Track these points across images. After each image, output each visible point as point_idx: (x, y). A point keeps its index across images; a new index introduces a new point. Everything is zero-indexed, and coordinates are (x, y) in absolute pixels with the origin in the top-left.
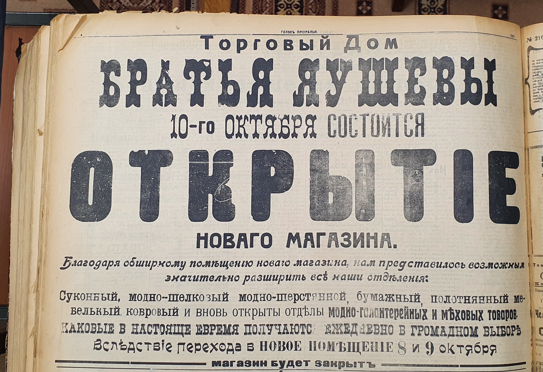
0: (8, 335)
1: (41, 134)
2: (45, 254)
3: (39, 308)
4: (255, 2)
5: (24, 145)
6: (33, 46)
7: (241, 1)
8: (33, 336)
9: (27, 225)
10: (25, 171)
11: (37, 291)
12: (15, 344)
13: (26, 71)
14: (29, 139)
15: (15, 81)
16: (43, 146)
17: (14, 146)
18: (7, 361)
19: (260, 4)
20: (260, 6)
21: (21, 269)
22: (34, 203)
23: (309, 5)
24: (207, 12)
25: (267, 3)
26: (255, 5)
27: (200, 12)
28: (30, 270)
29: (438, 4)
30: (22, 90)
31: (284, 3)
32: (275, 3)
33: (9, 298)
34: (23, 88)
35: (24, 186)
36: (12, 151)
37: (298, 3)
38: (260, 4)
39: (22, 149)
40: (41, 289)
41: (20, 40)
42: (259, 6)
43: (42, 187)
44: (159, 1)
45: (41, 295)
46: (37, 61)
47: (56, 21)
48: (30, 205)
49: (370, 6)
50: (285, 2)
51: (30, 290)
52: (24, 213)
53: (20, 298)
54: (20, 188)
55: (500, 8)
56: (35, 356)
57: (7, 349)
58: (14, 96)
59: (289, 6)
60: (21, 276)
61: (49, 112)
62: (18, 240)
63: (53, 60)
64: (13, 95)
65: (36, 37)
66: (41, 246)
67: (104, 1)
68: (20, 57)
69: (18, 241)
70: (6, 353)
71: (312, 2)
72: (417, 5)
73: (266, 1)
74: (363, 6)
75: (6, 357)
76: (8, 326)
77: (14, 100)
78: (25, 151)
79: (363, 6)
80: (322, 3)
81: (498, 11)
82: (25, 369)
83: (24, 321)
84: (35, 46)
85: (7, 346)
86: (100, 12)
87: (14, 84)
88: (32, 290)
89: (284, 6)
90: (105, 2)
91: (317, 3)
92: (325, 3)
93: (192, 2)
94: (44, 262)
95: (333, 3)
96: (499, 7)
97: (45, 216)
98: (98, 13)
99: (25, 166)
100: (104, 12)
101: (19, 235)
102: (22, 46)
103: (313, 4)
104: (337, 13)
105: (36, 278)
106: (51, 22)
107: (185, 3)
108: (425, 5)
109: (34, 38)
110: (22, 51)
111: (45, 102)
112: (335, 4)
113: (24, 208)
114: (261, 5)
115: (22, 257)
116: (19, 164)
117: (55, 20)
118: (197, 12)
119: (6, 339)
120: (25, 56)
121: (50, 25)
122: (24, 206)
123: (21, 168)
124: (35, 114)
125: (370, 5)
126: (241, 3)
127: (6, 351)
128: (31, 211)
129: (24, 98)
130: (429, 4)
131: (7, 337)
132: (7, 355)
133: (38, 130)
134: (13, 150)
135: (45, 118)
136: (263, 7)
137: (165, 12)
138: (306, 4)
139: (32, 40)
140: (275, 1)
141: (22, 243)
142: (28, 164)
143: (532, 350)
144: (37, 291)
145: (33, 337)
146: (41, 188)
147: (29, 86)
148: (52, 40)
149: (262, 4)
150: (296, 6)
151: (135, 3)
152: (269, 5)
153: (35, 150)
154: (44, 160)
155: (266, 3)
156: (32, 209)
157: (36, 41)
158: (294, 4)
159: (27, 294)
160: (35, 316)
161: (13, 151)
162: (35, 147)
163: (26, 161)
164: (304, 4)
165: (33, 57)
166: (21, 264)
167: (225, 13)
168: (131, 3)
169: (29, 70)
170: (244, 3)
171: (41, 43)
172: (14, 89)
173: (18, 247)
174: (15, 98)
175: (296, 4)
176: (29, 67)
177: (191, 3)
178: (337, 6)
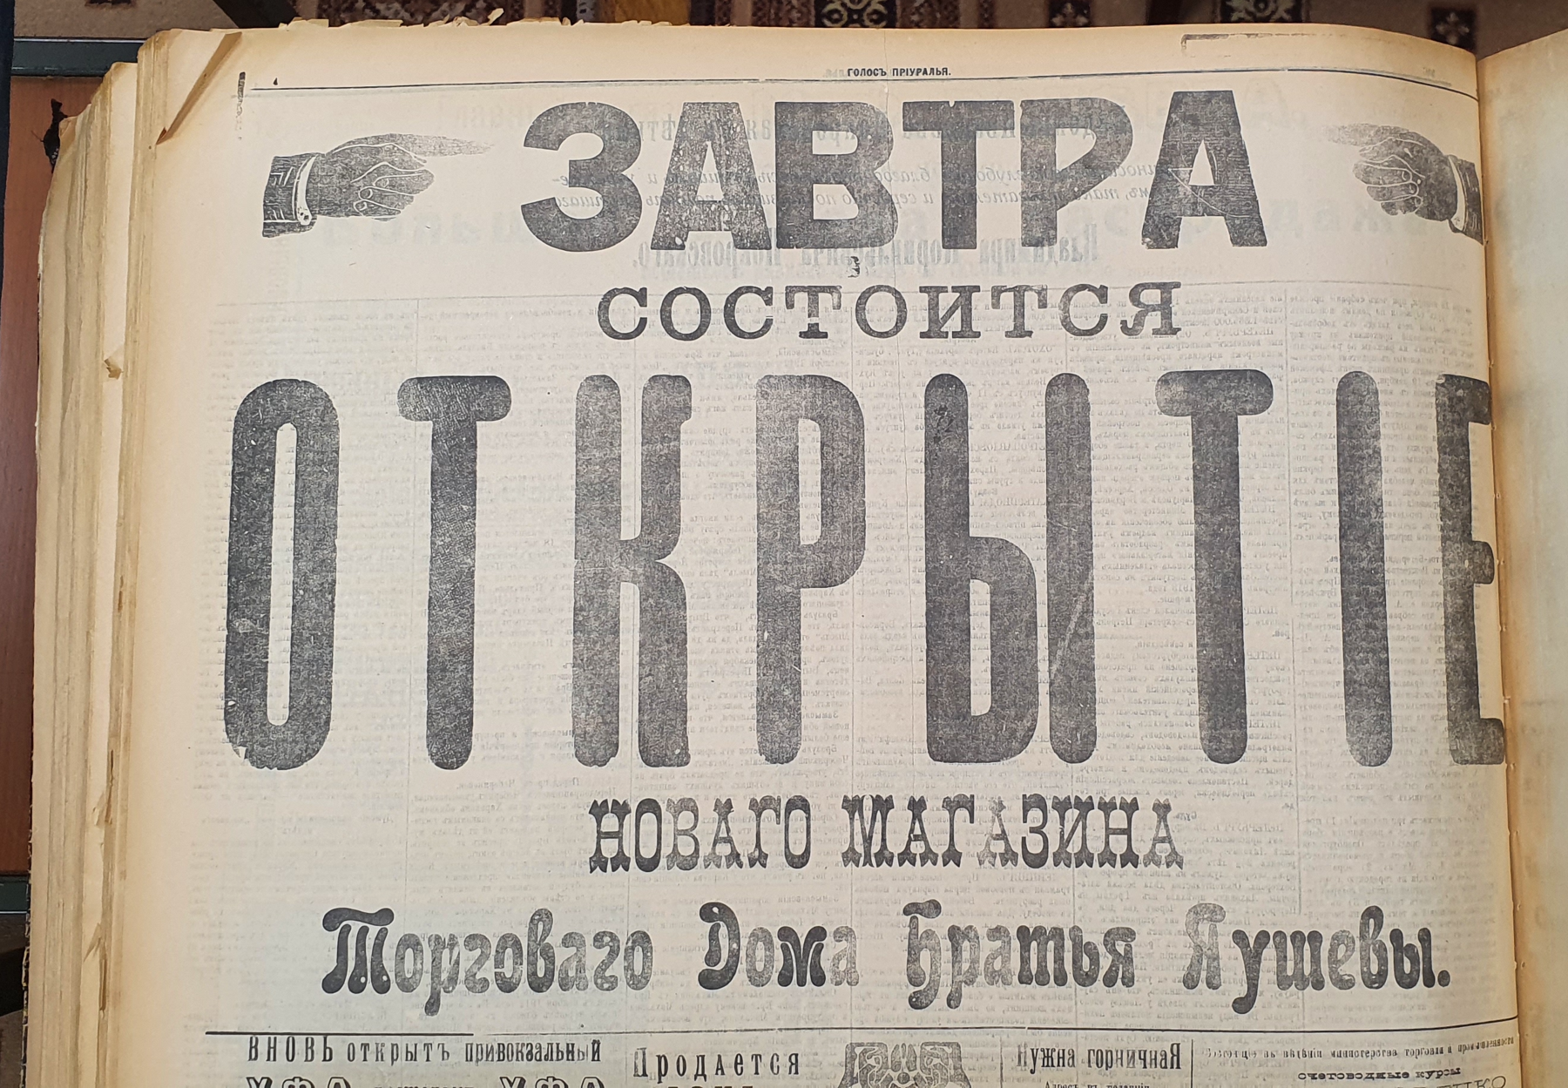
0: (28, 950)
1: (114, 373)
2: (129, 716)
3: (112, 869)
4: (759, 5)
5: (69, 408)
6: (90, 122)
7: (718, 4)
8: (96, 950)
9: (79, 636)
10: (71, 481)
11: (107, 819)
12: (49, 975)
13: (74, 198)
14: (83, 389)
15: (43, 225)
16: (121, 408)
17: (41, 409)
18: (26, 1022)
19: (772, 11)
20: (773, 16)
21: (64, 761)
22: (99, 569)
23: (913, 14)
24: (585, 22)
25: (793, 7)
26: (760, 14)
27: (567, 20)
28: (86, 761)
29: (1277, 8)
30: (62, 250)
31: (840, 8)
32: (816, 9)
33: (31, 844)
34: (66, 244)
35: (71, 524)
36: (36, 424)
37: (881, 8)
38: (772, 11)
39: (63, 418)
40: (117, 816)
41: (56, 106)
42: (769, 16)
43: (119, 525)
44: (485, 5)
45: (117, 834)
46: (103, 165)
47: (153, 48)
48: (87, 576)
49: (1084, 15)
50: (843, 5)
51: (89, 819)
52: (71, 599)
53: (62, 843)
54: (59, 529)
55: (1452, 18)
56: (103, 1008)
57: (27, 988)
58: (41, 267)
59: (855, 17)
60: (64, 779)
61: (136, 311)
62: (55, 676)
63: (145, 164)
64: (38, 265)
65: (98, 96)
66: (118, 694)
67: (330, 7)
68: (57, 156)
69: (55, 680)
70: (25, 1002)
71: (922, 5)
72: (1218, 11)
73: (790, 3)
74: (1065, 16)
75: (25, 1013)
76: (29, 923)
77: (39, 279)
78: (72, 423)
79: (1065, 16)
80: (950, 8)
81: (1446, 26)
82: (76, 1044)
83: (72, 907)
84: (97, 121)
85: (27, 980)
86: (281, 24)
87: (39, 233)
88: (94, 817)
89: (841, 15)
90: (331, 10)
91: (936, 6)
92: (956, 8)
93: (579, 9)
94: (127, 740)
95: (982, 6)
96: (1449, 15)
97: (125, 608)
98: (277, 26)
99: (73, 466)
100: (292, 23)
101: (59, 662)
102: (62, 124)
103: (922, 10)
104: (956, 18)
105: (105, 785)
106: (139, 53)
107: (558, 10)
108: (1241, 11)
109: (93, 101)
110: (62, 137)
111: (126, 282)
112: (986, 10)
113: (72, 586)
114: (776, 14)
115: (66, 725)
116: (57, 461)
117: (150, 47)
118: (557, 22)
119: (24, 962)
120: (71, 150)
121: (136, 62)
122: (72, 580)
123: (62, 473)
124: (98, 312)
125: (1085, 12)
126: (720, 8)
127: (25, 993)
128: (89, 594)
129: (67, 271)
130: (1252, 9)
131: (28, 955)
132: (27, 1007)
133: (106, 361)
134: (40, 421)
135: (127, 328)
136: (781, 19)
137: (466, 21)
138: (904, 10)
139: (90, 105)
140: (815, 2)
141: (66, 686)
142: (80, 464)
143: (1517, 970)
144: (107, 819)
145: (98, 952)
146: (117, 526)
147: (82, 237)
148: (145, 104)
149: (778, 10)
150: (875, 17)
151: (417, 10)
152: (799, 15)
153: (98, 421)
154: (125, 448)
155: (789, 7)
156: (91, 589)
157: (98, 110)
158: (869, 10)
159: (81, 829)
160: (103, 891)
161: (40, 424)
162: (98, 412)
163: (76, 451)
164: (899, 11)
165: (92, 154)
166: (65, 746)
167: (638, 22)
168: (406, 11)
169: (81, 190)
170: (729, 10)
171: (112, 113)
172: (39, 246)
173: (55, 698)
174: (43, 272)
175: (876, 12)
176: (80, 182)
177: (576, 10)
178: (991, 15)
